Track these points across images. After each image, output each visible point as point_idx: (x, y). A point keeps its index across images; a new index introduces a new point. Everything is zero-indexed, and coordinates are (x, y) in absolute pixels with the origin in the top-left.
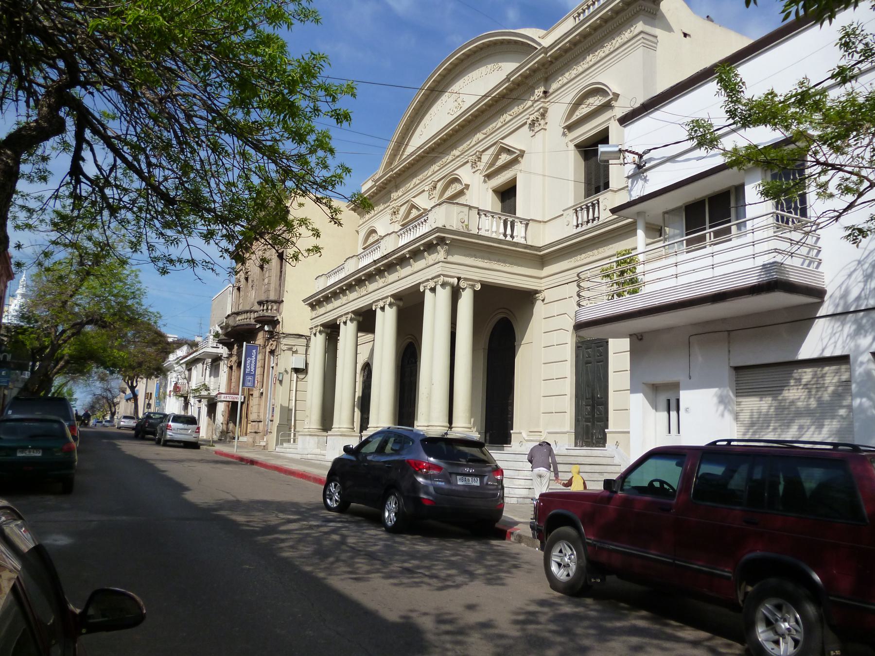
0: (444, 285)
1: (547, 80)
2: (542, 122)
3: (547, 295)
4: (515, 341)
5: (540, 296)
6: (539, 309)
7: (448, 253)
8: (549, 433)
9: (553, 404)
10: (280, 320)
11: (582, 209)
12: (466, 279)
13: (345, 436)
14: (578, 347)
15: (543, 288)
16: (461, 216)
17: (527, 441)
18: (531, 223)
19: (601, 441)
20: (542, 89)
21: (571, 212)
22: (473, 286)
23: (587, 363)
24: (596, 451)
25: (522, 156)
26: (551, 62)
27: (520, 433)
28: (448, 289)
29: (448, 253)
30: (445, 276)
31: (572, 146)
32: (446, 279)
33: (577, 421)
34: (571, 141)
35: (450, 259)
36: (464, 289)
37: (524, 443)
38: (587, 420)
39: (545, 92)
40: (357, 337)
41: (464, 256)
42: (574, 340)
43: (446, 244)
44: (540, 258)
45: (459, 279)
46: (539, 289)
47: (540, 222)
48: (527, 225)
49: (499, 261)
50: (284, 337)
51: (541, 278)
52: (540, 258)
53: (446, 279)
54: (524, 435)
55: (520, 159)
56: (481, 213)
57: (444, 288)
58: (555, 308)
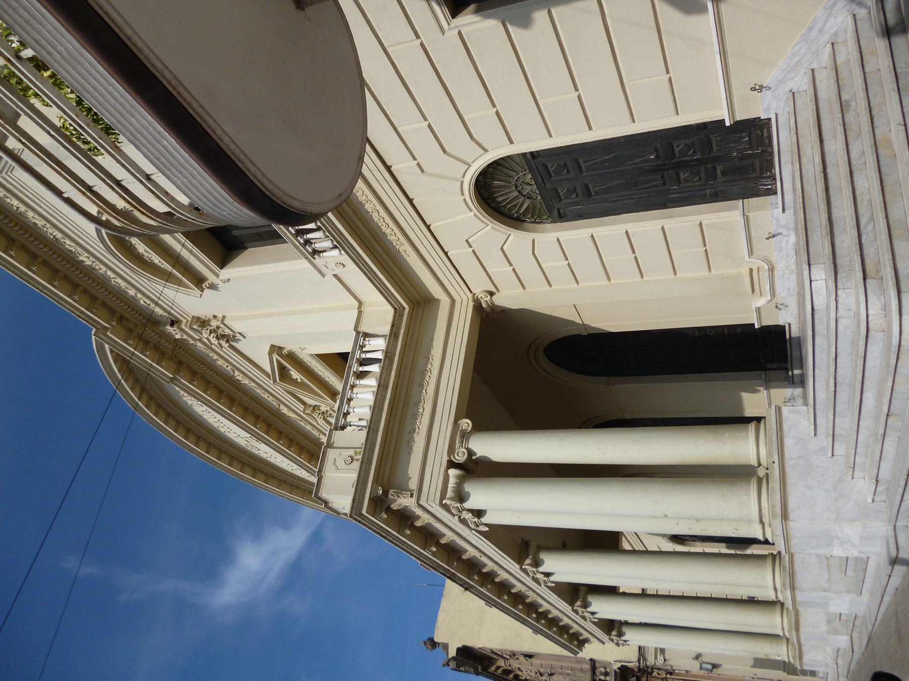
0: (461, 497)
1: (153, 321)
2: (214, 323)
3: (480, 286)
4: (579, 336)
5: (485, 300)
6: (510, 298)
7: (402, 489)
8: (751, 252)
9: (687, 249)
10: (619, 665)
11: (308, 242)
12: (451, 450)
13: (792, 576)
14: (562, 217)
15: (470, 296)
16: (341, 464)
17: (773, 295)
18: (364, 328)
19: (756, 131)
20: (169, 328)
21: (318, 261)
22: (465, 436)
23: (590, 195)
24: (783, 140)
25: (281, 348)
26: (121, 318)
27: (758, 310)
28: (468, 487)
29: (402, 489)
30: (443, 497)
31: (226, 273)
32: (450, 493)
33: (716, 197)
34: (217, 276)
35: (413, 484)
36: (471, 453)
37: (778, 300)
38: (712, 175)
39: (172, 325)
40: (634, 552)
41: (410, 454)
42: (549, 226)
43: (385, 493)
44: (416, 306)
45: (452, 464)
46: (471, 304)
47: (360, 313)
48: (366, 335)
49: (421, 385)
50: (645, 659)
51: (453, 301)
52: (416, 306)
53: (450, 493)
54: (761, 302)
55: (285, 352)
56: (342, 422)
57: (469, 494)
58: (499, 269)
